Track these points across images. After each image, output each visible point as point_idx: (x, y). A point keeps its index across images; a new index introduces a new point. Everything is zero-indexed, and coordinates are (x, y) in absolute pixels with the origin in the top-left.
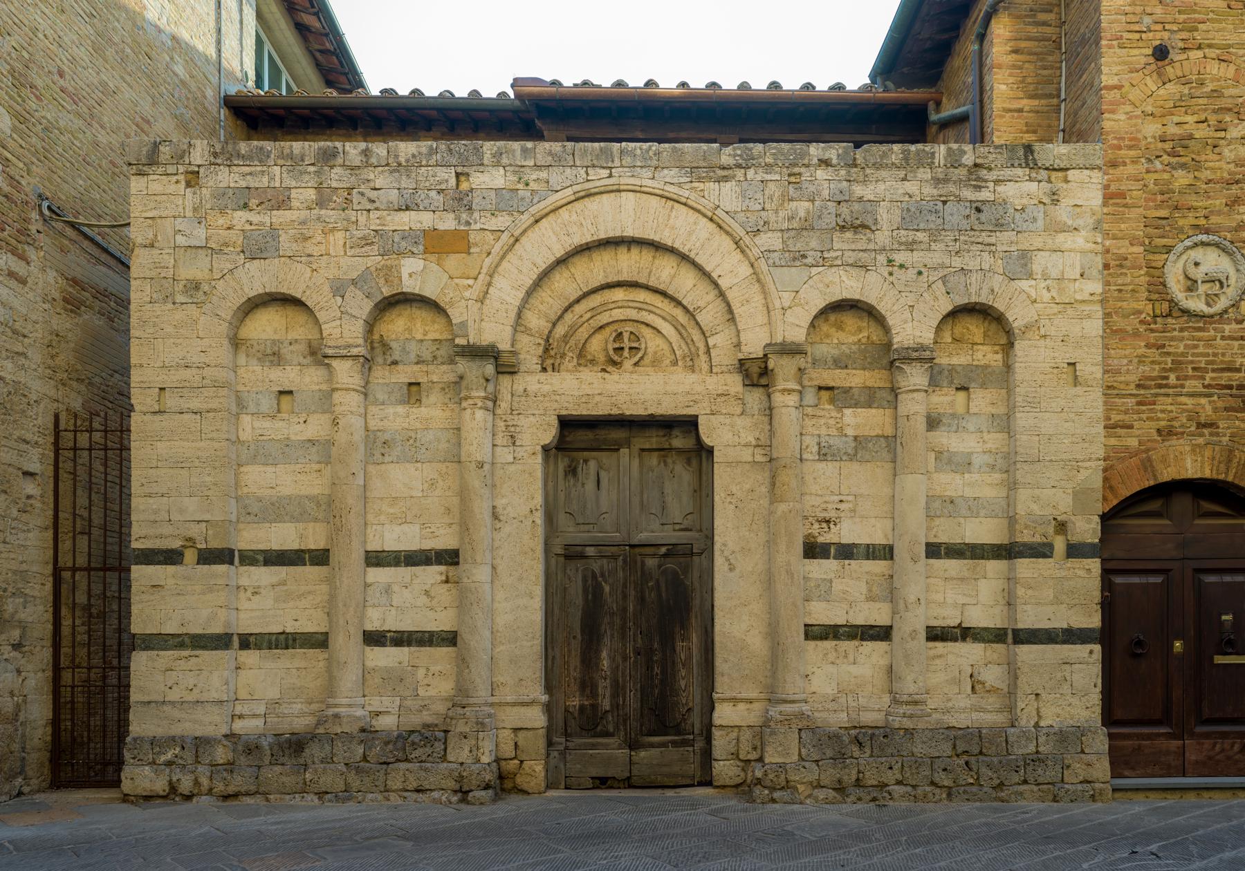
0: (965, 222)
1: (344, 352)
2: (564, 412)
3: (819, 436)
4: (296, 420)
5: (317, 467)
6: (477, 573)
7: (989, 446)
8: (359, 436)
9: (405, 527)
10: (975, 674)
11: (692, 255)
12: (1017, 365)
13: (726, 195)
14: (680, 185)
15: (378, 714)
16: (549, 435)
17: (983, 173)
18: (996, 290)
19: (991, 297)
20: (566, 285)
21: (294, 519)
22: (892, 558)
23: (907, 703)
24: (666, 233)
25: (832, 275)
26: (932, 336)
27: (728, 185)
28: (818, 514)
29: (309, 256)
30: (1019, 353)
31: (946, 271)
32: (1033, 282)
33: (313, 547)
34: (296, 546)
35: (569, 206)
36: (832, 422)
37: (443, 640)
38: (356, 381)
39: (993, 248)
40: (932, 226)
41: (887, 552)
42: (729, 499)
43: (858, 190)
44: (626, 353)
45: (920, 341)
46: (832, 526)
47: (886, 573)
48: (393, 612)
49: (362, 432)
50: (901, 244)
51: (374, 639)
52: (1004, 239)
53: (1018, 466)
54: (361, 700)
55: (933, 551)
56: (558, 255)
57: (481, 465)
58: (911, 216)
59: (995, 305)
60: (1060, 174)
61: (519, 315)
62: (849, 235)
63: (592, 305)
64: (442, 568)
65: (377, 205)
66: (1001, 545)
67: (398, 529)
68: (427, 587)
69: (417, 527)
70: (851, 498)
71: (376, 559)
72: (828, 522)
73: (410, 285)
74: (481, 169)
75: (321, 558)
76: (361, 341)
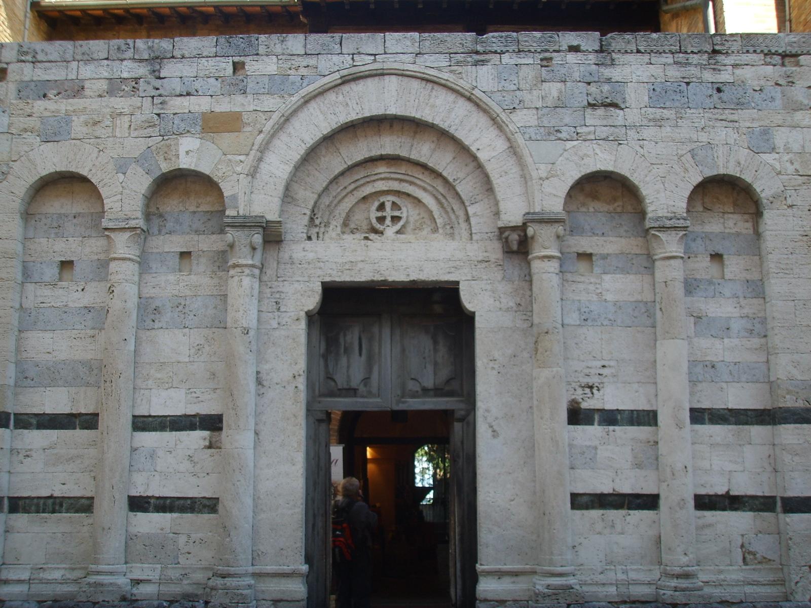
0: (708, 101)
1: (123, 225)
2: (327, 279)
3: (579, 301)
4: (75, 288)
5: (91, 332)
6: (239, 438)
7: (745, 311)
8: (133, 302)
9: (172, 392)
10: (747, 545)
11: (452, 131)
12: (768, 233)
13: (483, 79)
14: (439, 69)
15: (137, 582)
16: (313, 301)
17: (720, 58)
18: (742, 162)
19: (738, 169)
20: (335, 162)
21: (67, 384)
22: (656, 424)
23: (678, 576)
24: (427, 111)
25: (586, 148)
26: (684, 205)
27: (485, 68)
28: (581, 380)
29: (97, 138)
30: (769, 222)
31: (694, 146)
32: (777, 156)
33: (83, 411)
34: (67, 410)
35: (336, 89)
36: (592, 287)
37: (205, 506)
38: (132, 252)
39: (737, 125)
40: (677, 104)
41: (648, 418)
42: (491, 364)
43: (607, 72)
44: (388, 221)
45: (674, 209)
46: (595, 391)
47: (651, 439)
48: (157, 477)
49: (135, 300)
50: (650, 120)
51: (138, 504)
52: (745, 117)
53: (776, 331)
54: (122, 567)
55: (698, 416)
56: (325, 132)
57: (246, 332)
58: (659, 94)
59: (743, 177)
60: (792, 59)
61: (287, 188)
62: (601, 111)
63: (356, 177)
64: (206, 433)
65: (161, 92)
66: (764, 410)
67: (164, 394)
68: (190, 453)
69: (183, 391)
70: (612, 363)
71: (142, 424)
72: (591, 387)
73: (185, 163)
74: (255, 58)
75: (90, 421)
76: (139, 214)
